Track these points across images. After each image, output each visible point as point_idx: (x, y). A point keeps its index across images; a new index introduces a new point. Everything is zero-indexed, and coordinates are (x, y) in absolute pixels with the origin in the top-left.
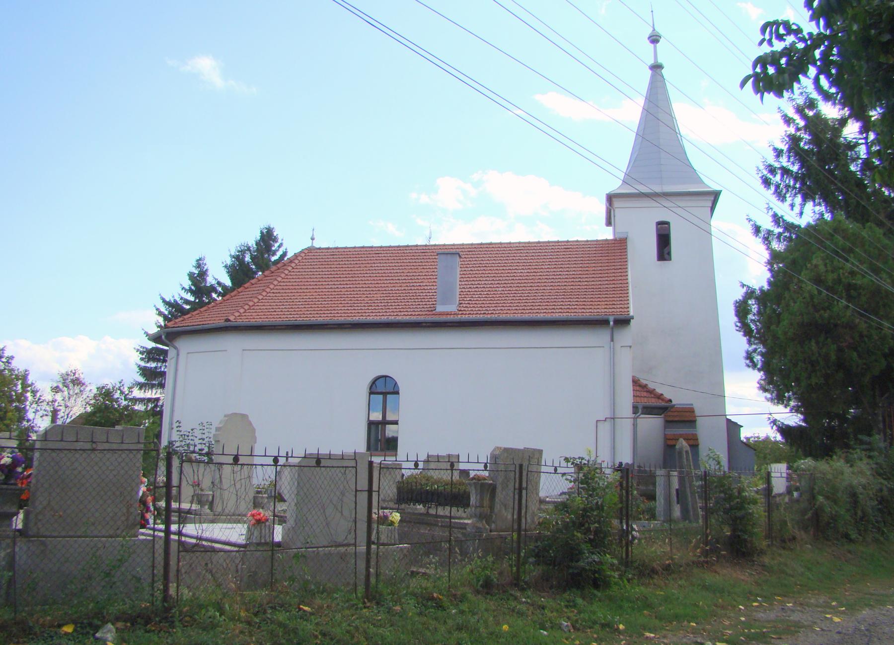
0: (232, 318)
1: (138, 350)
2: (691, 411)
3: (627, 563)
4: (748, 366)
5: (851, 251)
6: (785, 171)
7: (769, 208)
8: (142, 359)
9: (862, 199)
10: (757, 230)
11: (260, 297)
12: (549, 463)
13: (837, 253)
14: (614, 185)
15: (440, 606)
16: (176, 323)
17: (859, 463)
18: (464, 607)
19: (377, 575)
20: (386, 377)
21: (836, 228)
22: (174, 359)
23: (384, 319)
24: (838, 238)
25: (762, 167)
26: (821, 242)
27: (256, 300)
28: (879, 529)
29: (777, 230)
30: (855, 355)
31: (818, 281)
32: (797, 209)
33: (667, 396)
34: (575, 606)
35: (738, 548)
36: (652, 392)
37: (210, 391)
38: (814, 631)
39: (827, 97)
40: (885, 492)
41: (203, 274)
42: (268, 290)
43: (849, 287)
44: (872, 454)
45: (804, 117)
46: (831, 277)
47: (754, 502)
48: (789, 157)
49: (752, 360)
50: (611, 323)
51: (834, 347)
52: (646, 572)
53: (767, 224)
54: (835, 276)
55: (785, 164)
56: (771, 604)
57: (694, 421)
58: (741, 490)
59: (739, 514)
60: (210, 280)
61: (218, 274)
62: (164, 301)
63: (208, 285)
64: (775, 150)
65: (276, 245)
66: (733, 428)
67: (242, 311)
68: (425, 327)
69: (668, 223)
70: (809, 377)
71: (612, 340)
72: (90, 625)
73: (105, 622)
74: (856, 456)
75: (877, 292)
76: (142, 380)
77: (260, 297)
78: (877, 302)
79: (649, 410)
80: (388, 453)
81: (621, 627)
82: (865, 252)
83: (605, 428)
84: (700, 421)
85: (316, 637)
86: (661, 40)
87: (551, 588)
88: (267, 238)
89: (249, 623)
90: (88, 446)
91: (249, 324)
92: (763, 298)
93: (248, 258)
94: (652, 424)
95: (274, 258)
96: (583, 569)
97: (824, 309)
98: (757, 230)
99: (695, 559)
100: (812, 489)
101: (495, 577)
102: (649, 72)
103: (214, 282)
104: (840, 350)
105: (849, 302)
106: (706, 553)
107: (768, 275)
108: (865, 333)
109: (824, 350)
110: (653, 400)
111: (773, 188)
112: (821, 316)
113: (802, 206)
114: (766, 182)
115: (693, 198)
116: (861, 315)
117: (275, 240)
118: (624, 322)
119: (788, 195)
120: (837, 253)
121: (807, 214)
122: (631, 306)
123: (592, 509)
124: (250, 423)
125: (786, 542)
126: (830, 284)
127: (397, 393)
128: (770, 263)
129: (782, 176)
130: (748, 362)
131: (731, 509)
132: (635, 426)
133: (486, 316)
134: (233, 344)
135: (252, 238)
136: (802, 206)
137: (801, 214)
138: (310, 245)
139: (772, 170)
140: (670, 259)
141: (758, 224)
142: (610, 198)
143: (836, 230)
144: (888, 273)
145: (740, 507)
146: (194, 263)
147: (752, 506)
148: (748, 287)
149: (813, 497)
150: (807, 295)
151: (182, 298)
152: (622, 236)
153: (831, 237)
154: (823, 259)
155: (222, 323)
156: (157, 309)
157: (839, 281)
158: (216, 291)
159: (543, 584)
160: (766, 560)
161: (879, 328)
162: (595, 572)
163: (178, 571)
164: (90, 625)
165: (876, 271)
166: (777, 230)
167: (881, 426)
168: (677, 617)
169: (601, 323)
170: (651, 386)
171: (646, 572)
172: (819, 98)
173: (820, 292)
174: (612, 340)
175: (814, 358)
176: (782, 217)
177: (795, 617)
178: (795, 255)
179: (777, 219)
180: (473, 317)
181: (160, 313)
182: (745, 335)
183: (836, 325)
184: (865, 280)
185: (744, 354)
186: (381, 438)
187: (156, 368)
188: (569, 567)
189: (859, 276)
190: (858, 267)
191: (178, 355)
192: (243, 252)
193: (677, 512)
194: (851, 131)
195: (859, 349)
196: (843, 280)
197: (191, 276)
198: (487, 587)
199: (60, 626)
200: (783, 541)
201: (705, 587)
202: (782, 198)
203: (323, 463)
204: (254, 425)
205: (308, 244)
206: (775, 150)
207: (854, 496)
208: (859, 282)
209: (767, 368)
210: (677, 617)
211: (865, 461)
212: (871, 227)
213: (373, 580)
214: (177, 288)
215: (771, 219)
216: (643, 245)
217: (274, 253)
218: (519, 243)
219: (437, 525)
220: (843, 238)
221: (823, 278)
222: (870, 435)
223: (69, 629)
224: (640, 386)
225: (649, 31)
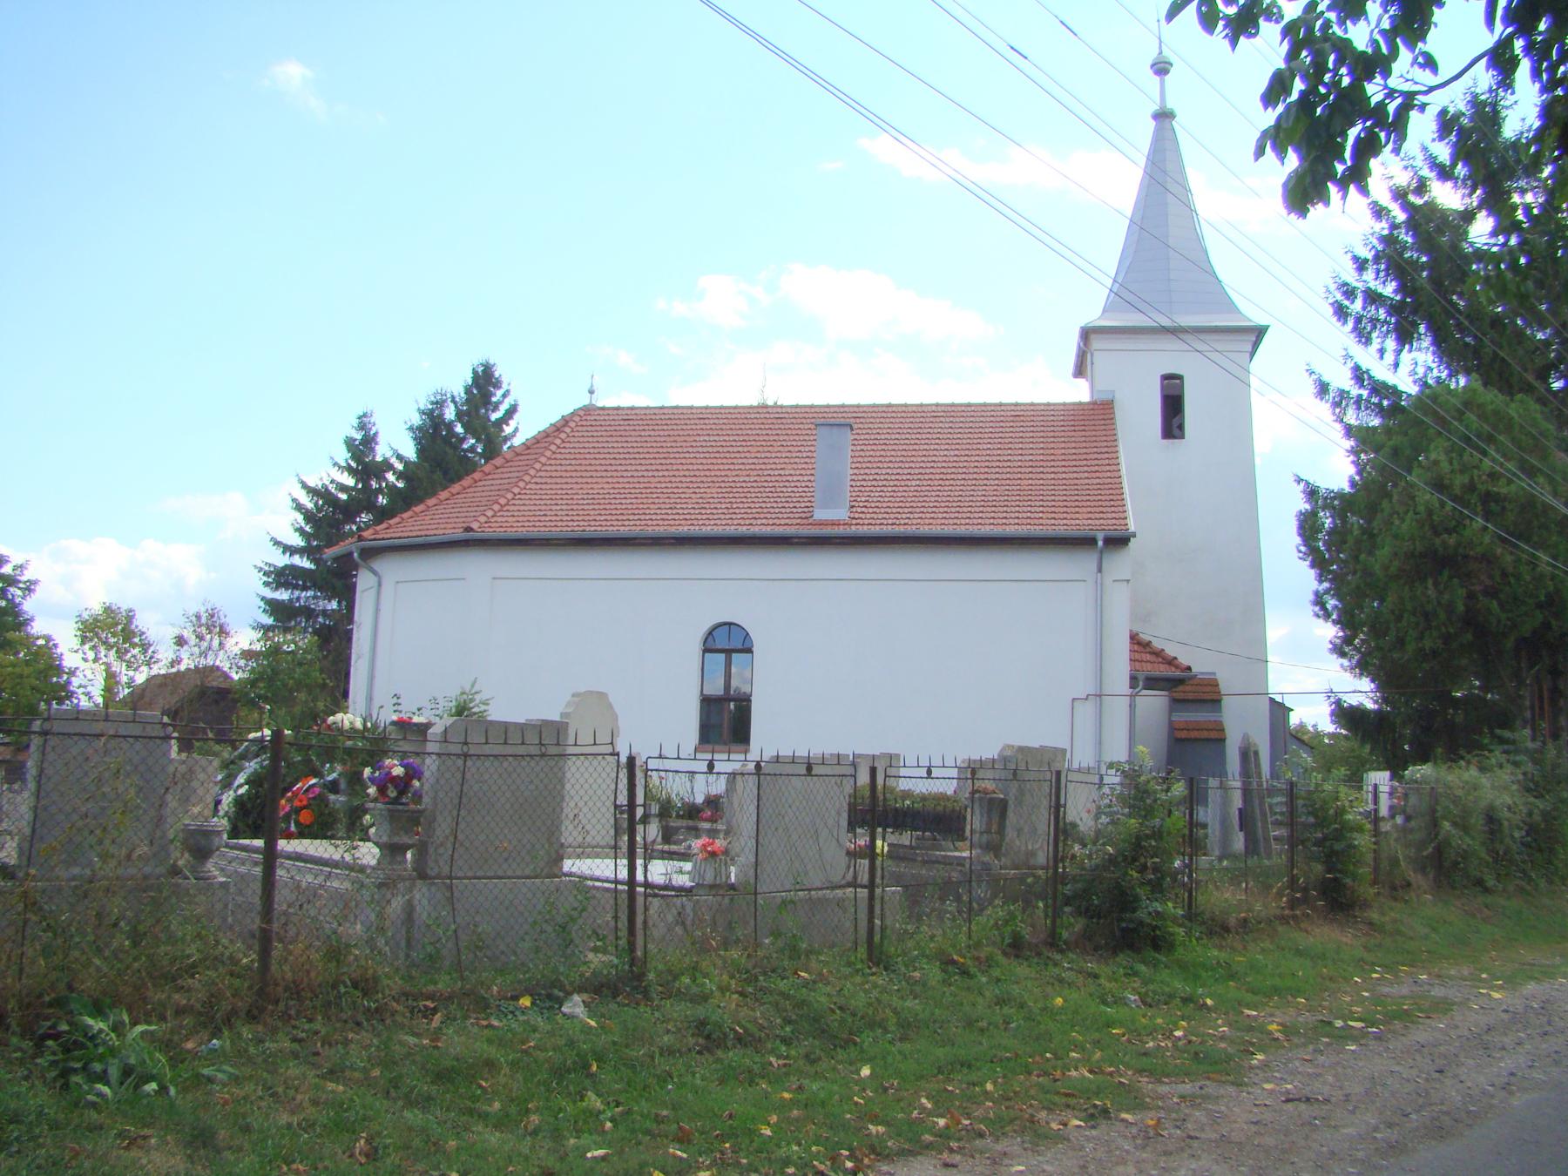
0: (475, 526)
1: (261, 569)
2: (1213, 684)
3: (1192, 915)
4: (1317, 616)
5: (1490, 439)
6: (1372, 297)
7: (1347, 357)
8: (267, 584)
9: (1501, 348)
10: (1322, 389)
11: (516, 490)
12: (911, 761)
13: (1467, 440)
14: (1092, 311)
15: (965, 973)
16: (376, 533)
17: (1499, 772)
18: (996, 972)
19: (883, 929)
20: (730, 624)
21: (1468, 402)
22: (373, 592)
23: (731, 530)
24: (1471, 417)
25: (1333, 287)
26: (1442, 422)
27: (510, 496)
28: (1524, 871)
29: (1355, 391)
30: (1495, 605)
31: (1439, 486)
32: (1389, 357)
33: (1184, 660)
34: (1136, 974)
35: (1336, 899)
36: (1159, 654)
37: (426, 646)
38: (1471, 1009)
39: (1444, 173)
40: (1537, 818)
41: (369, 441)
42: (527, 478)
43: (1487, 498)
44: (1518, 758)
45: (1407, 207)
46: (1459, 480)
47: (1360, 829)
48: (1378, 272)
49: (1322, 605)
50: (1100, 543)
51: (1462, 592)
52: (1218, 929)
53: (1341, 379)
54: (1466, 479)
55: (1373, 285)
56: (1396, 976)
57: (1219, 701)
58: (1341, 812)
59: (1338, 847)
60: (382, 452)
61: (397, 444)
62: (304, 486)
63: (379, 459)
64: (1355, 259)
65: (499, 393)
66: (1279, 711)
67: (490, 513)
68: (797, 544)
69: (1180, 378)
70: (1421, 638)
71: (1100, 570)
72: (550, 997)
73: (569, 994)
74: (1493, 761)
75: (1528, 503)
76: (269, 621)
77: (516, 490)
78: (1528, 522)
79: (1152, 683)
80: (733, 747)
81: (1209, 1002)
82: (1513, 440)
83: (1086, 712)
84: (1225, 701)
85: (833, 1011)
86: (1172, 70)
87: (1096, 950)
88: (484, 382)
89: (741, 994)
90: (534, 750)
91: (502, 536)
92: (1342, 504)
93: (450, 413)
94: (1154, 703)
95: (494, 416)
96: (1141, 923)
97: (1449, 531)
98: (1322, 389)
99: (1278, 912)
100: (1434, 811)
101: (1026, 932)
102: (1153, 123)
103: (389, 454)
104: (1471, 596)
105: (1487, 520)
106: (1293, 904)
107: (1352, 470)
108: (1510, 570)
109: (1446, 596)
110: (1162, 667)
111: (1350, 324)
112: (1444, 542)
113: (1398, 352)
114: (1341, 312)
115: (1232, 337)
116: (1504, 540)
117: (498, 385)
118: (1119, 541)
119: (1374, 335)
120: (1467, 440)
121: (1412, 368)
122: (1130, 514)
123: (1148, 837)
124: (610, 706)
125: (1397, 889)
126: (1457, 491)
127: (749, 651)
128: (1354, 452)
129: (1365, 301)
130: (1317, 609)
131: (1325, 838)
132: (1132, 706)
133: (897, 528)
134: (478, 569)
135: (457, 383)
136: (1398, 352)
137: (1396, 365)
138: (586, 402)
139: (1349, 293)
140: (1182, 437)
141: (1325, 379)
142: (1087, 334)
143: (1468, 404)
144: (1547, 476)
145: (1339, 835)
146: (355, 422)
147: (1355, 835)
148: (1307, 483)
149: (1435, 824)
150: (1421, 509)
151: (332, 482)
152: (1104, 397)
153: (1460, 415)
154: (1447, 452)
155: (459, 534)
156: (294, 500)
157: (1471, 487)
158: (391, 467)
159: (1088, 943)
160: (1374, 915)
161: (1533, 563)
162: (1155, 928)
163: (645, 922)
164: (550, 997)
165: (1530, 471)
166: (1355, 391)
167: (1528, 714)
168: (1276, 990)
169: (1086, 542)
170: (1157, 644)
171: (1218, 929)
172: (1432, 175)
173: (1443, 505)
174: (1100, 570)
175: (1429, 608)
176: (1367, 372)
177: (1438, 992)
178: (1395, 435)
179: (1359, 375)
180: (876, 530)
181: (299, 507)
182: (1312, 566)
183: (1466, 557)
184: (1513, 487)
185: (1312, 597)
186: (726, 720)
187: (291, 600)
188: (1120, 920)
189: (1503, 481)
190: (1501, 465)
191: (380, 585)
192: (440, 404)
193: (1239, 842)
194: (1481, 230)
195: (1502, 596)
196: (1479, 486)
197: (350, 443)
198: (1016, 947)
199: (516, 998)
200: (1394, 888)
201: (1299, 953)
202: (1364, 338)
203: (816, 770)
204: (617, 709)
205: (584, 401)
206: (1355, 259)
207: (1491, 819)
208: (1504, 491)
209: (1347, 621)
210: (1276, 990)
211: (1509, 768)
212: (1521, 402)
213: (877, 938)
214: (328, 467)
215: (1349, 374)
216: (1140, 413)
217: (496, 408)
218: (937, 405)
219: (914, 860)
220: (1479, 417)
221: (1446, 482)
222: (1512, 729)
223: (526, 1001)
224: (1139, 643)
225: (1152, 55)
